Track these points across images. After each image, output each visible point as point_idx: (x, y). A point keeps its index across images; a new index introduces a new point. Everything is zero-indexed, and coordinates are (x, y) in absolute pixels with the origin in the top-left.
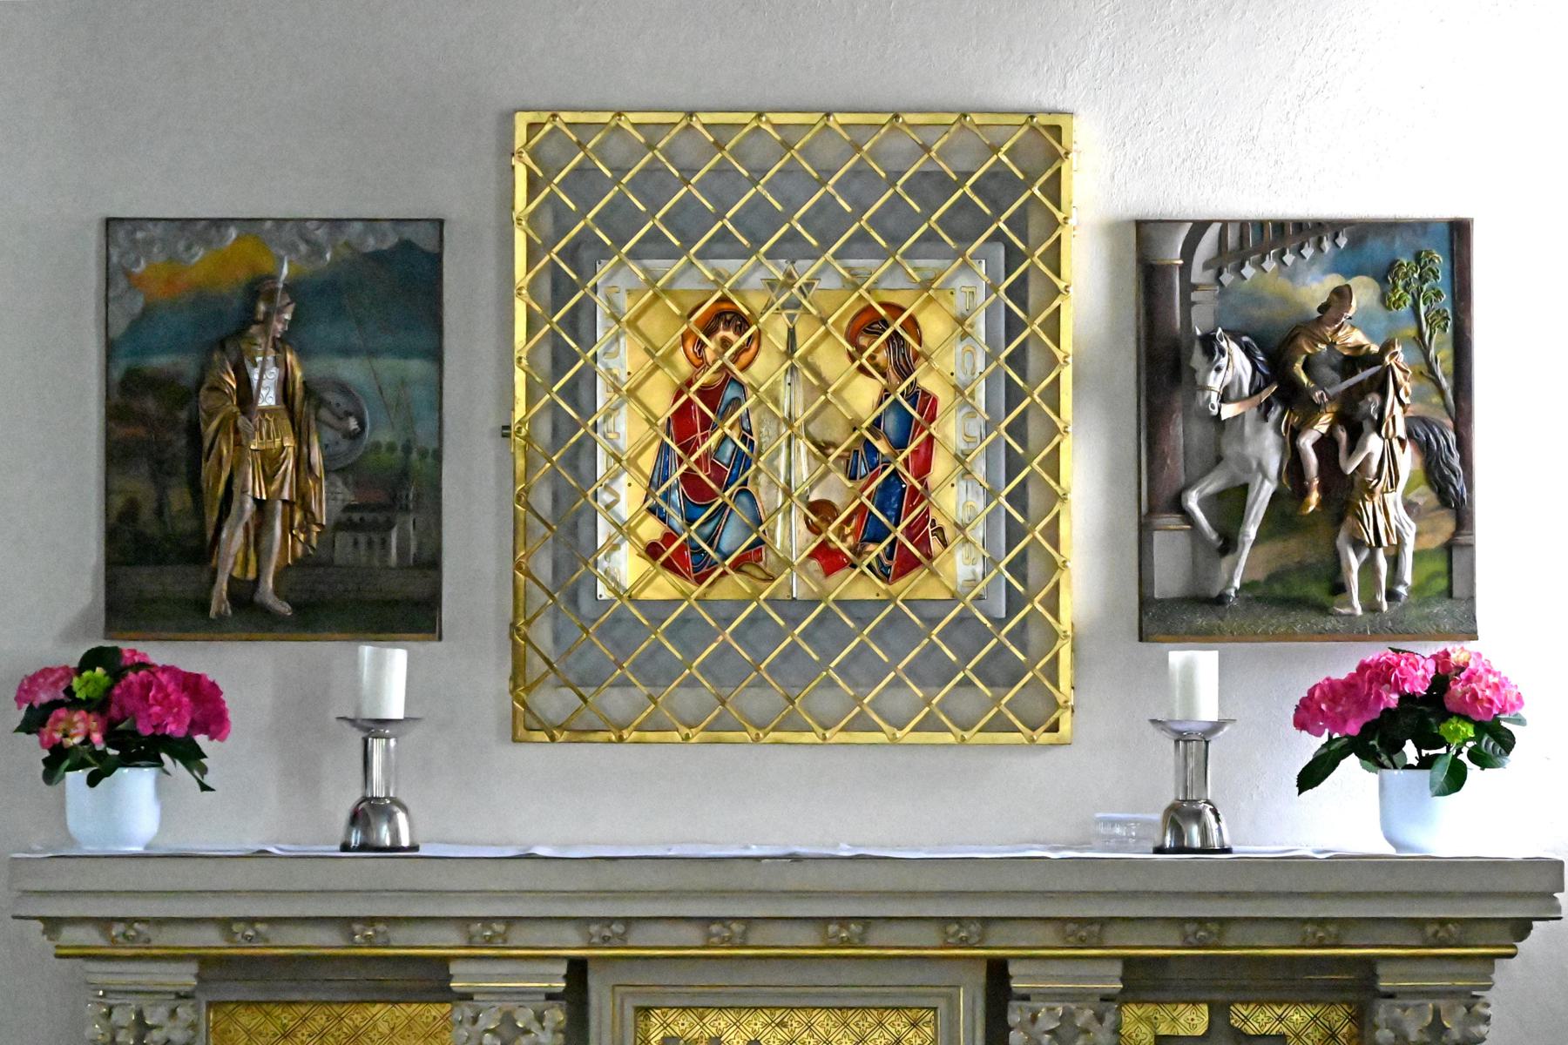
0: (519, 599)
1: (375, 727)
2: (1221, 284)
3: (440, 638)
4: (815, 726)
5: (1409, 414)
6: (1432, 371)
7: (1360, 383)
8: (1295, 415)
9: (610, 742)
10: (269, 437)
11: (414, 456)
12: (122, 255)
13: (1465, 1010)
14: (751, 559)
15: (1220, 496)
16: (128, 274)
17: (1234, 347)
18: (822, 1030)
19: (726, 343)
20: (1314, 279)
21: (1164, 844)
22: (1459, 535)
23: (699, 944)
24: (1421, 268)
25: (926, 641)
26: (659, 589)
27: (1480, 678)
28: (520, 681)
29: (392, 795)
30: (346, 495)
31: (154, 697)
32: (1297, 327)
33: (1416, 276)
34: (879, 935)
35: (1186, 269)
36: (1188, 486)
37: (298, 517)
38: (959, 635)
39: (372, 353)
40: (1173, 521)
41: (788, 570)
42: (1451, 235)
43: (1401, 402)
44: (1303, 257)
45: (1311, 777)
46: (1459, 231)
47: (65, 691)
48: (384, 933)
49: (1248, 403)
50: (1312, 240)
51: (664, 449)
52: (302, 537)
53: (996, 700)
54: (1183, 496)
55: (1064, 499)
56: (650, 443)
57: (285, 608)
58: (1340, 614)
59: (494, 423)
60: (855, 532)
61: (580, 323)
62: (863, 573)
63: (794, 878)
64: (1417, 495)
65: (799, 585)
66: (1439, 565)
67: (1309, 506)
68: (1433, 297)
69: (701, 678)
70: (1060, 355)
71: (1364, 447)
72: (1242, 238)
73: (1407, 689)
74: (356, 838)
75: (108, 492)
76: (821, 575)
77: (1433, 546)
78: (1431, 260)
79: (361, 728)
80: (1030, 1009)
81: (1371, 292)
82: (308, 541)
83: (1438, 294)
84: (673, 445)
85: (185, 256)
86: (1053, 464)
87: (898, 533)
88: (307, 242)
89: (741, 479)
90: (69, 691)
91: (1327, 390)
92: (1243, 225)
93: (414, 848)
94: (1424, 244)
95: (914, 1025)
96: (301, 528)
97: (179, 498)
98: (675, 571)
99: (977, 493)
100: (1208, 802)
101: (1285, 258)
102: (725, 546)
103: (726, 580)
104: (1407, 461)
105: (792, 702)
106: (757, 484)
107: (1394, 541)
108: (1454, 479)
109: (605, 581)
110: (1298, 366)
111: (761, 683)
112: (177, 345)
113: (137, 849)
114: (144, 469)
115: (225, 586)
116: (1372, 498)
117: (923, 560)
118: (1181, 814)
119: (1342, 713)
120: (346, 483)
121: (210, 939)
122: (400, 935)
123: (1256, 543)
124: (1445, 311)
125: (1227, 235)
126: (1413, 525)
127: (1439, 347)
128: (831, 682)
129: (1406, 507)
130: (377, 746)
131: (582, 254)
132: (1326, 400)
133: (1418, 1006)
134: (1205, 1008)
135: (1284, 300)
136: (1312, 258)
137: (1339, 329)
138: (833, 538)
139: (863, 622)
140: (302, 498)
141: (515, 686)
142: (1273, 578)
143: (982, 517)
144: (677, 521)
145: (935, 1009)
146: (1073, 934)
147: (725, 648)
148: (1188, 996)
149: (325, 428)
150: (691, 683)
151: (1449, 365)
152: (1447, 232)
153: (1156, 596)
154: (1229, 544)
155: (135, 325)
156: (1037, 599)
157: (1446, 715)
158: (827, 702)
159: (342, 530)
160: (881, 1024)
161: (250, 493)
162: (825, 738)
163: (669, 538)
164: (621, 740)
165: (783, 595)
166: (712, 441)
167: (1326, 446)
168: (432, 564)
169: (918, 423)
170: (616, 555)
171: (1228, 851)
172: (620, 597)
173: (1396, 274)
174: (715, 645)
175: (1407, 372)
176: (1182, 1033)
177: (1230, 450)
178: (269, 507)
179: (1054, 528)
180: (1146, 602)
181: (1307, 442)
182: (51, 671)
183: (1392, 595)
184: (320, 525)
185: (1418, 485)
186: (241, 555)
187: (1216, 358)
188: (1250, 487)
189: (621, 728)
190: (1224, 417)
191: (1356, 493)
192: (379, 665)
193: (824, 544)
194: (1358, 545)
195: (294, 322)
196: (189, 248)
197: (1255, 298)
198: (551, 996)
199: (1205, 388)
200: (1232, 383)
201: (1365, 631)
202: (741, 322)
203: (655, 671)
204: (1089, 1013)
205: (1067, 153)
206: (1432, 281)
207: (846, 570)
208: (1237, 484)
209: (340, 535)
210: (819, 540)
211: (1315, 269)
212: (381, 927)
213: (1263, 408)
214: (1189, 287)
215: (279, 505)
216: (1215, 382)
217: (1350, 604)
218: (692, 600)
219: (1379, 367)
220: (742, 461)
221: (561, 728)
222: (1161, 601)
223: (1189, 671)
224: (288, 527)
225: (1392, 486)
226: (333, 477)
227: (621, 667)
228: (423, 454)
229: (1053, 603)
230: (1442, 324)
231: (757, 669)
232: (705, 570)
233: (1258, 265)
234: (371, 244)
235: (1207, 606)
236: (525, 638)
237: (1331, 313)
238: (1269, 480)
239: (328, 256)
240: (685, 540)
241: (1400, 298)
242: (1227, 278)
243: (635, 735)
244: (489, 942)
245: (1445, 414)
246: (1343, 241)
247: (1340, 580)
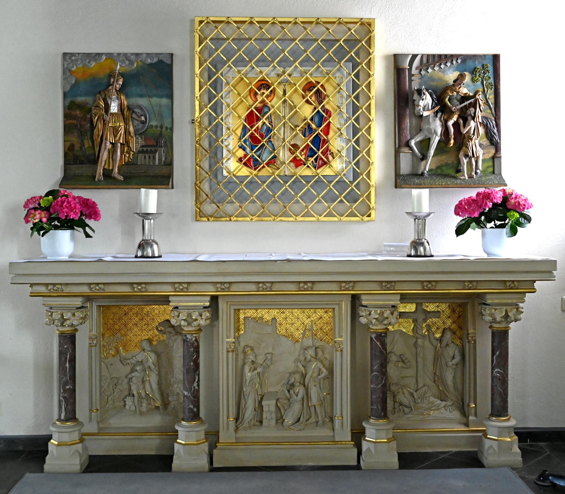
0: (197, 175)
1: (146, 216)
2: (421, 75)
3: (173, 188)
4: (293, 215)
6: (487, 102)
7: (465, 106)
9: (227, 221)
10: (115, 122)
11: (164, 129)
12: (68, 64)
13: (516, 310)
14: (272, 162)
15: (421, 142)
16: (70, 71)
17: (427, 93)
18: (296, 314)
19: (263, 93)
20: (451, 73)
21: (411, 254)
23: (256, 290)
25: (328, 188)
26: (244, 173)
27: (520, 197)
28: (198, 201)
29: (152, 239)
30: (141, 142)
31: (65, 206)
32: (446, 87)
34: (317, 286)
35: (410, 70)
36: (411, 139)
37: (126, 149)
38: (337, 187)
39: (150, 97)
40: (406, 150)
41: (284, 165)
44: (447, 66)
45: (460, 230)
46: (496, 58)
47: (38, 204)
48: (145, 288)
49: (431, 111)
50: (450, 60)
51: (244, 127)
52: (127, 155)
53: (351, 207)
54: (410, 142)
55: (372, 142)
56: (240, 126)
57: (121, 178)
58: (461, 179)
59: (189, 118)
60: (305, 154)
61: (216, 85)
62: (308, 166)
63: (288, 268)
65: (288, 169)
66: (491, 164)
69: (256, 200)
70: (371, 96)
71: (469, 125)
72: (428, 60)
73: (495, 201)
74: (140, 254)
75: (65, 141)
76: (294, 167)
77: (488, 158)
79: (142, 216)
80: (368, 310)
82: (129, 157)
83: (489, 78)
84: (247, 125)
85: (89, 65)
86: (369, 130)
87: (320, 153)
88: (129, 60)
89: (269, 136)
90: (39, 204)
91: (456, 107)
92: (428, 55)
93: (160, 257)
94: (485, 62)
95: (326, 312)
96: (127, 152)
97: (87, 143)
98: (248, 167)
99: (344, 141)
100: (425, 239)
101: (435, 68)
102: (263, 159)
103: (264, 169)
104: (481, 130)
105: (286, 208)
106: (274, 139)
109: (225, 169)
110: (447, 99)
111: (275, 202)
112: (87, 94)
113: (66, 258)
114: (76, 134)
115: (102, 172)
117: (328, 162)
118: (417, 244)
119: (473, 209)
120: (142, 138)
121: (85, 290)
122: (151, 288)
123: (433, 157)
126: (482, 151)
127: (490, 95)
128: (297, 202)
129: (479, 145)
130: (147, 222)
131: (217, 64)
133: (501, 308)
134: (415, 304)
135: (440, 79)
136: (450, 66)
137: (460, 87)
138: (299, 155)
139: (308, 182)
140: (127, 143)
141: (196, 203)
142: (438, 168)
143: (345, 149)
144: (248, 150)
145: (334, 309)
146: (385, 286)
147: (264, 190)
148: (411, 301)
149: (135, 120)
150: (253, 202)
151: (493, 100)
153: (401, 174)
154: (424, 157)
155: (73, 87)
156: (364, 174)
157: (509, 210)
158: (296, 208)
159: (140, 153)
160: (315, 312)
161: (109, 140)
162: (296, 219)
163: (245, 156)
164: (230, 220)
165: (282, 174)
166: (260, 123)
167: (456, 124)
168: (170, 164)
169: (325, 118)
170: (229, 162)
171: (432, 256)
172: (230, 174)
173: (476, 71)
174: (260, 189)
176: (407, 311)
177: (425, 127)
178: (115, 145)
179: (368, 153)
180: (397, 175)
181: (450, 123)
182: (35, 197)
183: (476, 173)
184: (133, 152)
186: (107, 161)
189: (230, 216)
191: (466, 140)
192: (147, 195)
193: (295, 158)
194: (466, 156)
195: (122, 85)
196: (89, 62)
197: (432, 79)
198: (205, 307)
199: (418, 105)
200: (426, 105)
202: (267, 86)
203: (241, 198)
204: (388, 312)
205: (373, 31)
206: (487, 74)
207: (302, 166)
209: (140, 155)
210: (294, 156)
211: (451, 70)
212: (143, 286)
214: (411, 75)
215: (119, 145)
216: (422, 103)
217: (464, 175)
218: (253, 108)
220: (269, 130)
221: (211, 216)
222: (403, 175)
223: (419, 197)
224: (122, 152)
226: (137, 136)
227: (230, 197)
228: (167, 128)
229: (368, 175)
231: (274, 197)
232: (257, 166)
233: (433, 68)
234: (149, 61)
235: (418, 177)
236: (199, 187)
237: (458, 82)
239: (135, 65)
240: (251, 156)
242: (423, 72)
243: (235, 219)
244: (182, 291)
245: (492, 116)
246: (459, 61)
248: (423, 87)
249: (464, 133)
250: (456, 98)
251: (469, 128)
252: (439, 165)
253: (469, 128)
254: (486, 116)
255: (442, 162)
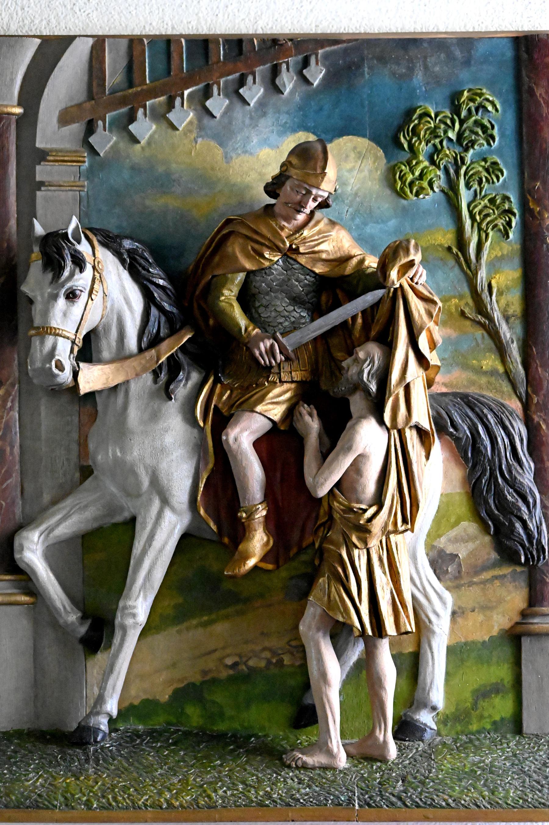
2: (93, 151)
5: (438, 388)
8: (225, 388)
20: (265, 142)
22: (535, 615)
24: (462, 122)
32: (229, 222)
33: (452, 135)
42: (517, 59)
43: (421, 359)
44: (245, 102)
49: (134, 363)
50: (261, 70)
58: (305, 767)
64: (456, 540)
67: (247, 557)
68: (484, 174)
78: (480, 107)
81: (368, 164)
107: (410, 626)
108: (524, 508)
116: (365, 542)
124: (506, 198)
125: (103, 62)
126: (448, 596)
127: (494, 267)
129: (433, 564)
132: (279, 357)
136: (262, 104)
152: (509, 54)
173: (415, 132)
175: (434, 303)
185: (457, 523)
187: (66, 273)
188: (139, 520)
190: (84, 388)
201: (350, 801)
208: (119, 519)
213: (163, 377)
219: (379, 293)
225: (405, 521)
230: (500, 222)
235: (54, 749)
238: (173, 510)
241: (421, 177)
245: (506, 387)
247: (307, 701)
248: (75, 221)
249: (322, 492)
250: (284, 284)
251: (347, 462)
252: (197, 678)
253: (347, 462)
254: (472, 390)
255: (211, 663)
